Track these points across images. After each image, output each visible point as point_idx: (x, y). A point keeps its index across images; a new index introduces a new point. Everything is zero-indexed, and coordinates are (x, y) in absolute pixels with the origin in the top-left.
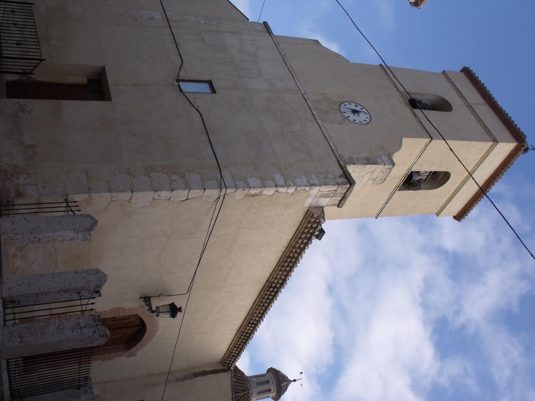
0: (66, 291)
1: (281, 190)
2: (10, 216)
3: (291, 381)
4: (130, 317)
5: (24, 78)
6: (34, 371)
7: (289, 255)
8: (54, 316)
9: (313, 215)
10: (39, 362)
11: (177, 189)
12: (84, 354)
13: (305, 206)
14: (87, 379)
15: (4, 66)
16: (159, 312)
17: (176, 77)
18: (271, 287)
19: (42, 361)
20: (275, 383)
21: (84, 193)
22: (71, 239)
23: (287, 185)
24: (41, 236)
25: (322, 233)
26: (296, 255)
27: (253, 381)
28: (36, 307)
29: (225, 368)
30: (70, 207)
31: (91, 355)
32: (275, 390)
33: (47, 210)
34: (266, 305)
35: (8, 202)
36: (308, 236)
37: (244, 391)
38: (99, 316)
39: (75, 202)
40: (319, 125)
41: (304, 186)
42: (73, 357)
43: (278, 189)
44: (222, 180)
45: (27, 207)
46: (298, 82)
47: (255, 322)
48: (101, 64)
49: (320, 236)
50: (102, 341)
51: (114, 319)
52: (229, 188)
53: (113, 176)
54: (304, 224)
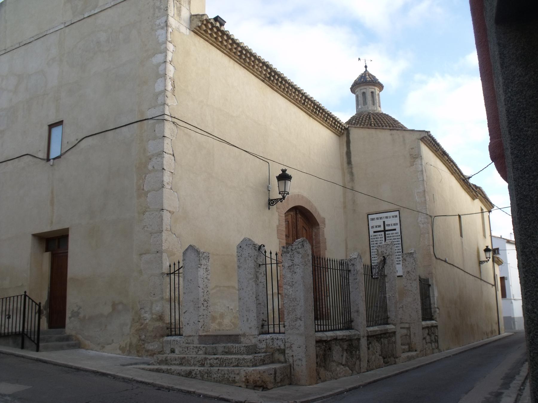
0: (257, 278)
1: (169, 58)
2: (181, 327)
3: (366, 70)
4: (287, 221)
5: (45, 312)
6: (329, 311)
7: (239, 56)
8: (280, 292)
9: (199, 27)
10: (321, 306)
11: (162, 164)
12: (318, 264)
13: (188, 34)
14: (341, 263)
15: (33, 329)
16: (285, 191)
17: (44, 162)
18: (269, 78)
19: (321, 304)
20: (365, 87)
21: (161, 257)
22: (207, 271)
23: (165, 50)
24: (202, 299)
25: (219, 19)
26: (239, 49)
27: (362, 108)
28: (270, 307)
30: (175, 271)
31: (320, 258)
32: (373, 87)
33: (177, 293)
34: (287, 85)
35: (167, 329)
36: (220, 34)
37: (370, 118)
38: (283, 247)
39: (170, 266)
40: (101, 11)
41: (167, 33)
42: (319, 276)
43: (168, 61)
44: (157, 118)
45: (173, 311)
46: (51, 31)
47: (304, 98)
48: (30, 238)
49: (222, 21)
50: (308, 246)
51: (287, 236)
52: (164, 111)
53: (146, 229)
54: (207, 37)
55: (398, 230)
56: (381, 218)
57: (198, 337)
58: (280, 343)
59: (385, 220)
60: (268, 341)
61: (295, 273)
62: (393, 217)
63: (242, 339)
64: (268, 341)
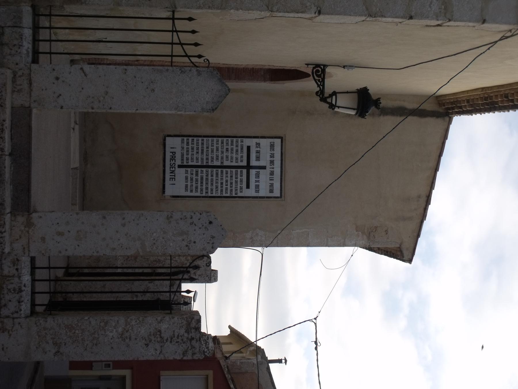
29: (441, 110)
55: (247, 193)
56: (272, 162)
57: (27, 105)
58: (12, 306)
59: (268, 170)
60: (16, 279)
61: (147, 345)
62: (272, 185)
63: (21, 219)
64: (16, 279)
